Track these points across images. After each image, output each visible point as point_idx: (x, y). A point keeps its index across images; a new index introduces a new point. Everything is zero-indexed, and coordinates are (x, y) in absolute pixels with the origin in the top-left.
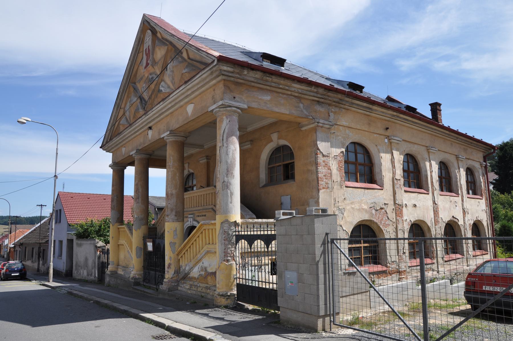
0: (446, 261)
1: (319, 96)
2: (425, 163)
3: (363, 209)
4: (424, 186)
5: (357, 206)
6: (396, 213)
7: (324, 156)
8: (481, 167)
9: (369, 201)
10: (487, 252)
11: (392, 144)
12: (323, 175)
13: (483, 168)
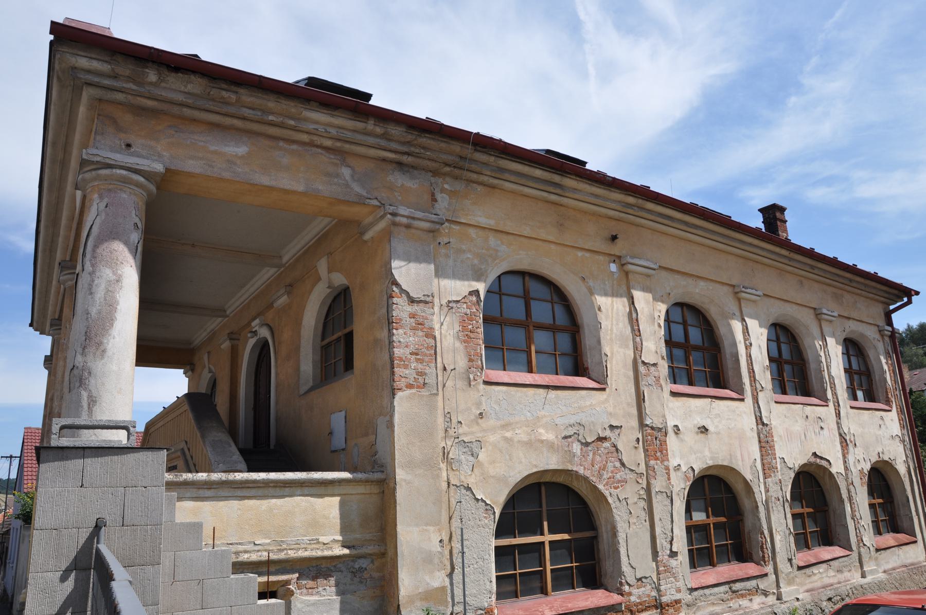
0: (800, 568)
1: (394, 146)
2: (729, 325)
3: (542, 442)
4: (732, 381)
5: (521, 434)
6: (646, 451)
7: (412, 301)
8: (882, 336)
9: (559, 421)
10: (914, 539)
11: (631, 276)
12: (408, 351)
13: (887, 339)
